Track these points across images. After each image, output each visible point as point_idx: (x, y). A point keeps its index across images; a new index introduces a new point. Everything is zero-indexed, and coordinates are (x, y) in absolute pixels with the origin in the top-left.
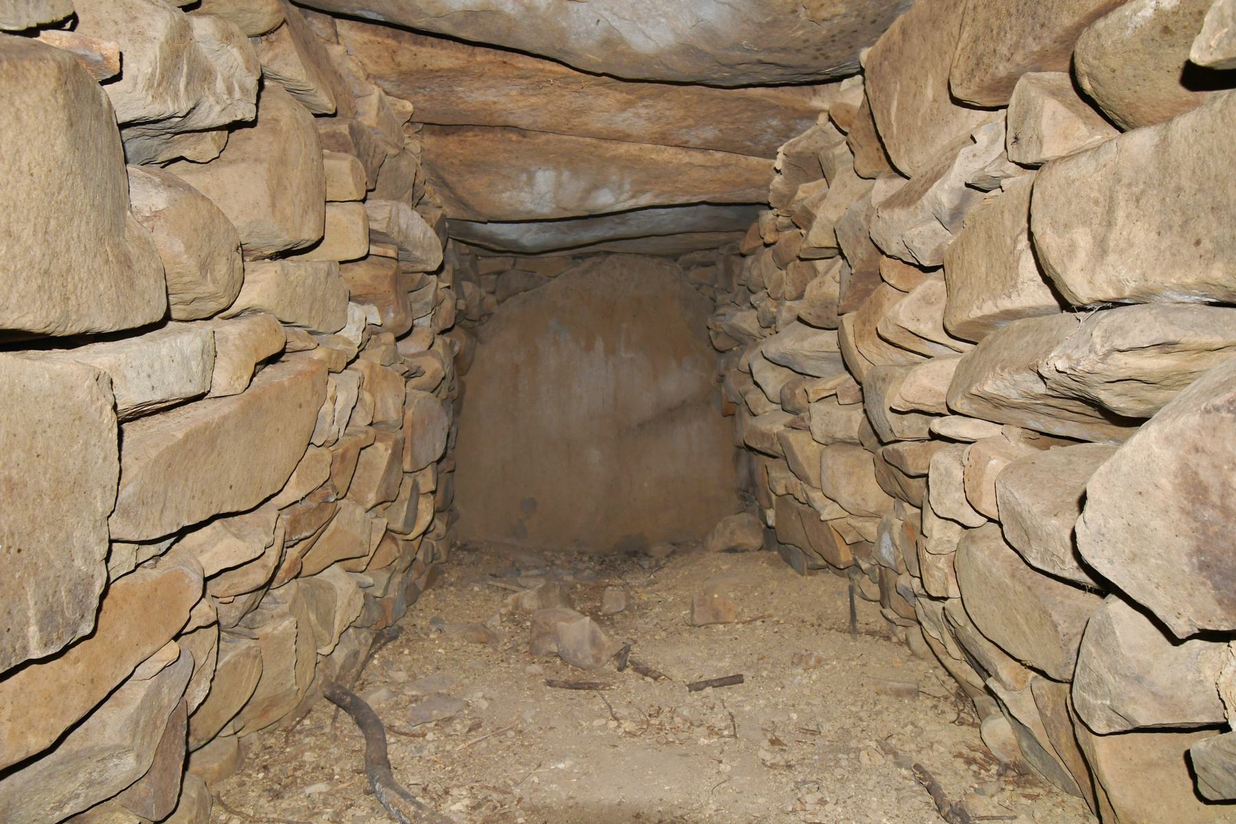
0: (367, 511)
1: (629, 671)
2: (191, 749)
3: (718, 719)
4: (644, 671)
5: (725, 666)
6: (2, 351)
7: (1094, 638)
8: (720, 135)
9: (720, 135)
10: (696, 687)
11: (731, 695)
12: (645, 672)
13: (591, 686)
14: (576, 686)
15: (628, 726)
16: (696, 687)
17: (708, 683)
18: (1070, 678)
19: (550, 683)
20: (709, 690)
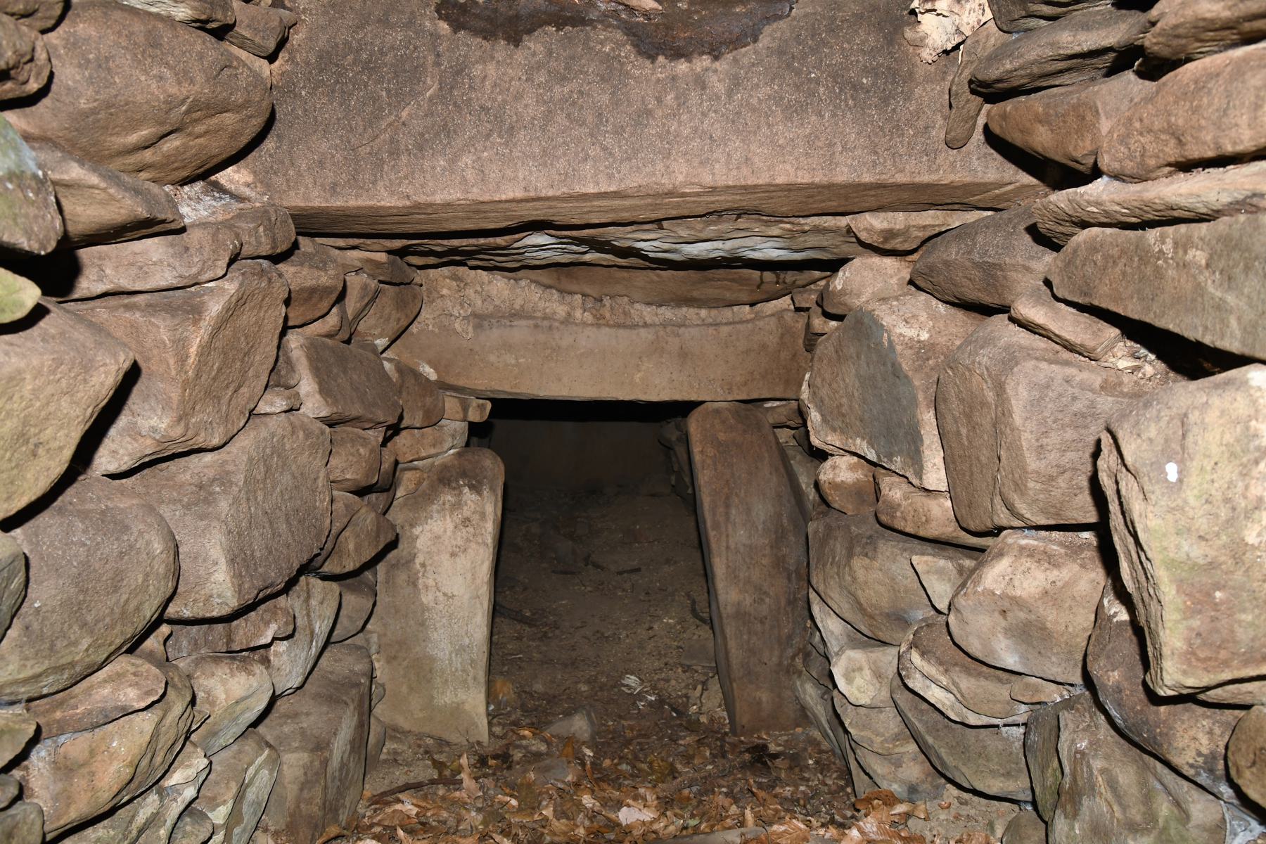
0: (397, 463)
1: (590, 566)
2: (166, 616)
3: (628, 586)
4: (596, 566)
5: (635, 563)
6: (7, 267)
7: (976, 379)
8: (927, 55)
9: (927, 55)
10: (620, 573)
11: (634, 577)
12: (596, 566)
13: (573, 573)
14: (565, 573)
15: (589, 589)
16: (620, 573)
17: (625, 572)
18: (497, 620)
19: (553, 572)
20: (625, 575)
